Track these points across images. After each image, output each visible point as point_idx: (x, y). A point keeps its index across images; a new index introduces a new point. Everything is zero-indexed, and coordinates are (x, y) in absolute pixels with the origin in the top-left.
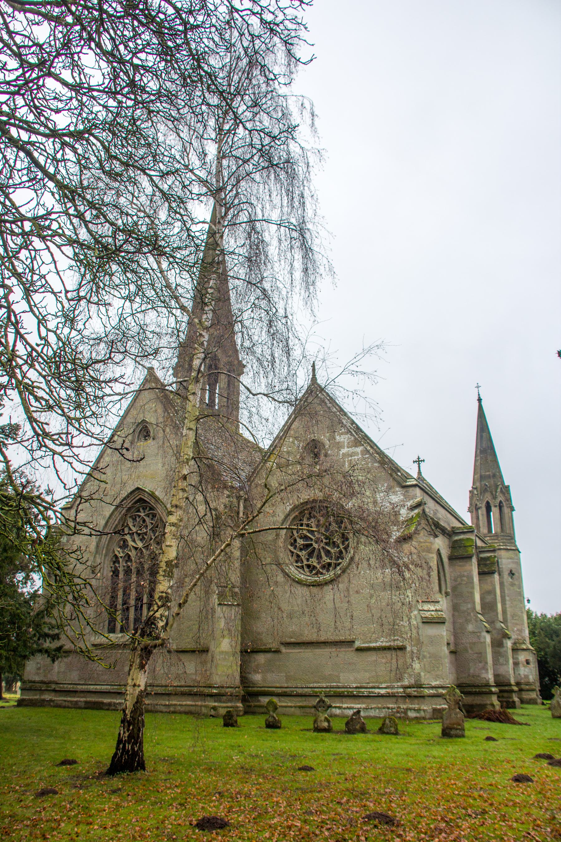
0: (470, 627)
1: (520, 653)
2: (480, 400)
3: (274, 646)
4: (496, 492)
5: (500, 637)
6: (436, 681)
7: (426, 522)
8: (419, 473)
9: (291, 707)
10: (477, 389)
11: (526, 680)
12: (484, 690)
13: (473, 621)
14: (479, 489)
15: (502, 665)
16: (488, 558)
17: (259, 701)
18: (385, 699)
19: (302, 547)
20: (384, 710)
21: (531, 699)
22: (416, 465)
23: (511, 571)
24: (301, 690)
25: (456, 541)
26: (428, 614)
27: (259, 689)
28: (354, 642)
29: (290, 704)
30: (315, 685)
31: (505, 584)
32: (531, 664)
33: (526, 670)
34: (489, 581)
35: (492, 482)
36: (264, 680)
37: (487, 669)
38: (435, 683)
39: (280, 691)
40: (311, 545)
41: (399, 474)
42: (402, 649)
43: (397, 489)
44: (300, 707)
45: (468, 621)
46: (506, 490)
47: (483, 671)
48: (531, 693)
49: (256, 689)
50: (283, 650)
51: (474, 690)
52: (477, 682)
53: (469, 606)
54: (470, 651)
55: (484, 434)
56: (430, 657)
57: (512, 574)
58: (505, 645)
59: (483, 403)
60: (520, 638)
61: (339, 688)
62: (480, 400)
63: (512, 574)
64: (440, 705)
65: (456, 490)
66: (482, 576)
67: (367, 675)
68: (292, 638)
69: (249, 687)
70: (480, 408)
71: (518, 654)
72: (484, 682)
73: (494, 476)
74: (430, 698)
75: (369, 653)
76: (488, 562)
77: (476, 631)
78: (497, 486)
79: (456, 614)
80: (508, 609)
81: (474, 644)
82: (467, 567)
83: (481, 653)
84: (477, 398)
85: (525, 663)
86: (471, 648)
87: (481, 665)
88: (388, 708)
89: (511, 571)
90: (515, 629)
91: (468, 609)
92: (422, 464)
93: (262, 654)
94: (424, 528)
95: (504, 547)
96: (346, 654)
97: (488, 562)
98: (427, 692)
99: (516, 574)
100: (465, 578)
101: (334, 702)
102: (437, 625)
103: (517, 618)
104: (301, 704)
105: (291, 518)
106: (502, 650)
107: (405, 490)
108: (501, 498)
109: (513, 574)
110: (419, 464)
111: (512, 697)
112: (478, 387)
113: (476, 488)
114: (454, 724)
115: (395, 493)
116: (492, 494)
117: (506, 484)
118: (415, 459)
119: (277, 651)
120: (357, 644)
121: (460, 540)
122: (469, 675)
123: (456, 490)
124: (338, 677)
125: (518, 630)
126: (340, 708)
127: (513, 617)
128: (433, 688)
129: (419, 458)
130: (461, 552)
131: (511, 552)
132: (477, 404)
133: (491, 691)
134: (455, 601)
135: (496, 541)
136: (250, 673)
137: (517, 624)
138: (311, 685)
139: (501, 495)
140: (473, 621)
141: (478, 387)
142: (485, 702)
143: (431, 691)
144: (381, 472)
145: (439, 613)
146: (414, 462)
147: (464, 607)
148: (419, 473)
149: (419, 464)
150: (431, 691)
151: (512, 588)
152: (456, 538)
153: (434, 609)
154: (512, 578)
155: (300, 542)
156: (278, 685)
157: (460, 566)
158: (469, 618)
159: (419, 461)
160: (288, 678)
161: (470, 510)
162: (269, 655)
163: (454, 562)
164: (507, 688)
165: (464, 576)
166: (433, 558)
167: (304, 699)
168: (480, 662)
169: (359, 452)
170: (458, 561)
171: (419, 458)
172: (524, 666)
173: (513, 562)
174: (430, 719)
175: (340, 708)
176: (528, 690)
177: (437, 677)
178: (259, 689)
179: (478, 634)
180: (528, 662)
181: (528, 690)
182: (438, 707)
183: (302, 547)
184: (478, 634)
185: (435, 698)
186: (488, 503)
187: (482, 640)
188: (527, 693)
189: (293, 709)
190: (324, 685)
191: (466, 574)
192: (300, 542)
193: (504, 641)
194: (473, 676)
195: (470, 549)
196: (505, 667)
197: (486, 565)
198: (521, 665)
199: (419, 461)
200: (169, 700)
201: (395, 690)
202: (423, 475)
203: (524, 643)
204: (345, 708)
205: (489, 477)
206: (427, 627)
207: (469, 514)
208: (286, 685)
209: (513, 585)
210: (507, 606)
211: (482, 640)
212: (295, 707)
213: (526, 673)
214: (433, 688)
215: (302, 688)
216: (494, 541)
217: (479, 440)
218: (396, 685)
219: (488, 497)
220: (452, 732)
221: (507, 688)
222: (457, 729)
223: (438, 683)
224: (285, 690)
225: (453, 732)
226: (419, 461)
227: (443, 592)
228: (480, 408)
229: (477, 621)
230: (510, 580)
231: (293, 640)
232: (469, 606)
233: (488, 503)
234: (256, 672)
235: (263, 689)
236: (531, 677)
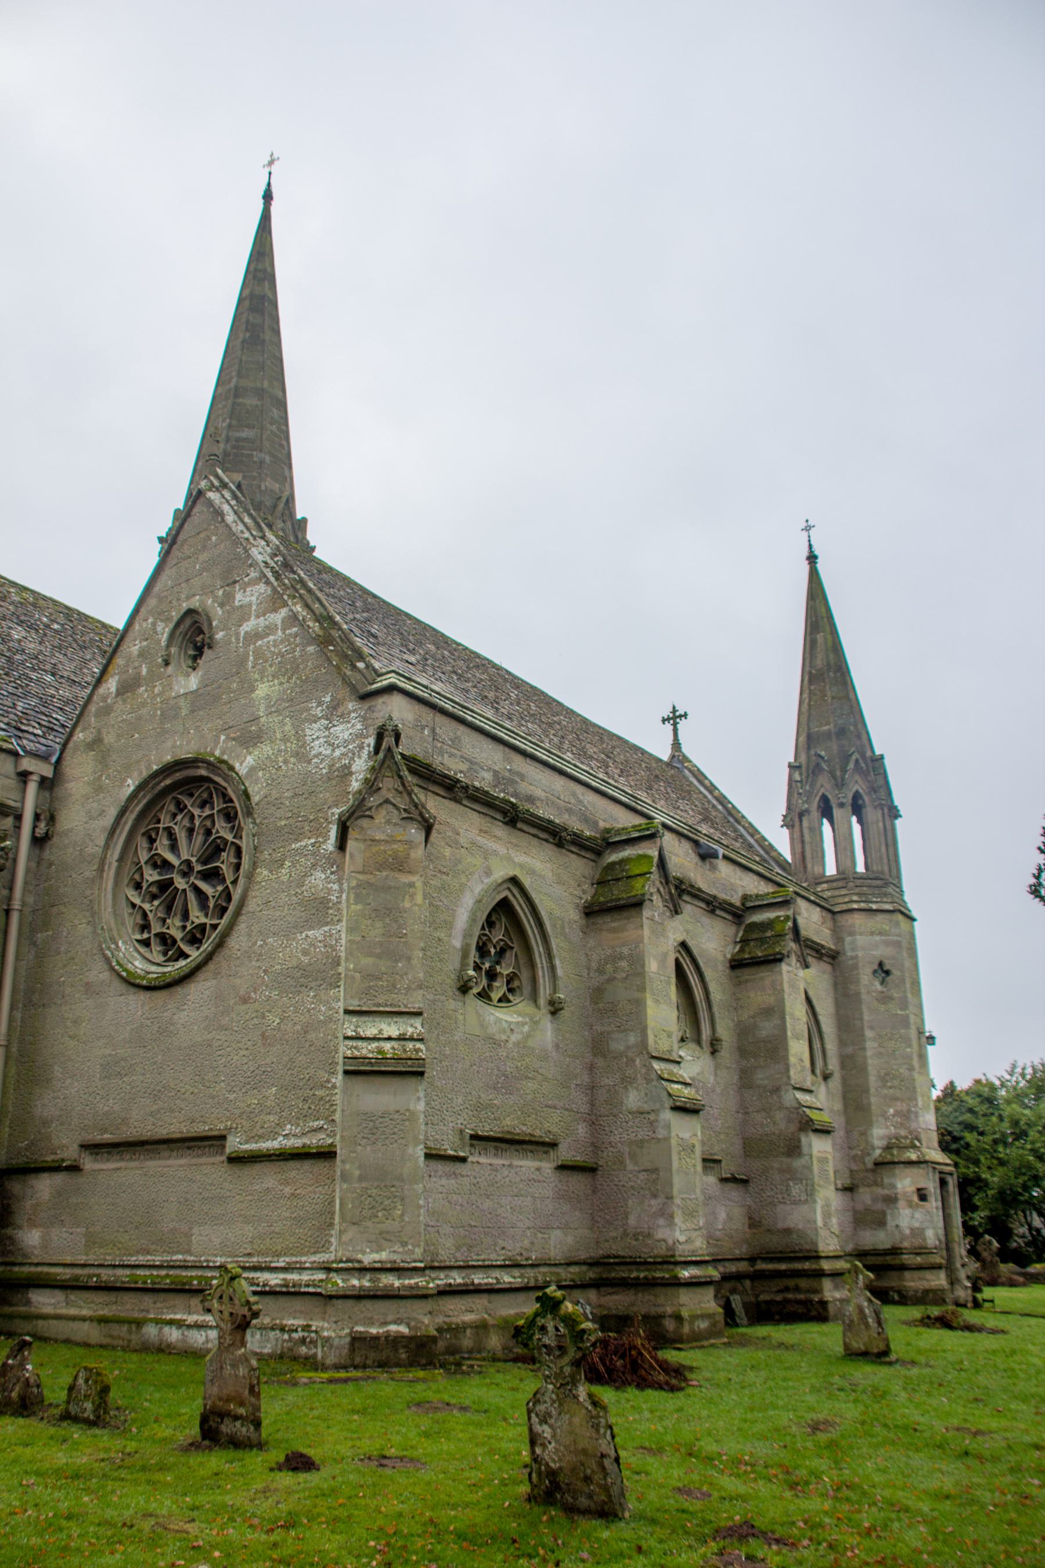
0: (633, 1099)
1: (899, 1170)
2: (812, 558)
3: (70, 1152)
4: (844, 770)
5: (793, 1127)
6: (380, 1249)
7: (398, 784)
8: (676, 745)
9: (83, 1319)
10: (805, 534)
11: (917, 1242)
12: (658, 1275)
13: (640, 1080)
14: (804, 769)
15: (796, 1203)
16: (769, 925)
17: (28, 1302)
18: (283, 1301)
19: (154, 889)
20: (272, 1334)
21: (927, 1292)
22: (669, 727)
23: (881, 964)
24: (110, 1271)
25: (614, 863)
26: (367, 1049)
27: (33, 1269)
28: (223, 1138)
29: (85, 1312)
30: (142, 1259)
31: (864, 996)
32: (932, 1199)
33: (917, 1215)
34: (767, 982)
35: (835, 747)
36: (45, 1244)
37: (672, 1216)
38: (376, 1256)
39: (65, 1273)
40: (171, 882)
41: (361, 665)
42: (327, 1155)
43: (350, 706)
44: (103, 1320)
45: (627, 1081)
46: (875, 766)
47: (661, 1221)
48: (928, 1275)
49: (26, 1269)
50: (88, 1163)
51: (634, 1275)
52: (646, 1252)
53: (632, 1039)
54: (630, 1166)
55: (820, 637)
56: (361, 1179)
57: (883, 971)
58: (805, 1150)
59: (820, 566)
60: (903, 1133)
61: (186, 1267)
62: (812, 558)
63: (883, 971)
64: (385, 1323)
65: (753, 774)
66: (738, 972)
67: (249, 1230)
68: (105, 1130)
69: (14, 1264)
70: (814, 577)
71: (894, 1176)
72: (661, 1251)
73: (841, 732)
74: (350, 1303)
75: (257, 1168)
76: (769, 934)
77: (646, 1107)
78: (847, 757)
79: (600, 1062)
80: (870, 1061)
81: (640, 1144)
82: (630, 933)
83: (656, 1170)
84: (805, 553)
85: (916, 1199)
86: (633, 1156)
87: (655, 1204)
88: (282, 1329)
89: (881, 964)
90: (891, 1111)
91: (628, 1048)
92: (682, 724)
93: (45, 1175)
94: (387, 801)
95: (863, 905)
96: (209, 1171)
97: (769, 934)
98: (685, 1274)
99: (896, 972)
100: (623, 964)
101: (173, 1309)
102: (396, 1083)
103: (896, 1083)
104: (104, 1312)
105: (133, 816)
106: (798, 1163)
107: (366, 705)
108: (857, 785)
109: (887, 973)
110: (675, 725)
111: (818, 1291)
112: (808, 528)
113: (799, 767)
114: (228, 1400)
115: (344, 717)
116: (834, 777)
117: (878, 752)
118: (667, 712)
119: (74, 1168)
120: (235, 1144)
121: (622, 862)
122: (625, 1234)
123: (753, 774)
124: (188, 1235)
125: (897, 1113)
126: (179, 1324)
127: (883, 1079)
128: (363, 1270)
129: (674, 711)
130: (618, 893)
131: (880, 917)
132: (805, 568)
133: (676, 1277)
134: (599, 1028)
135: (843, 892)
136: (20, 1228)
137: (896, 1099)
138: (133, 1260)
139: (857, 777)
140: (640, 1080)
141: (808, 528)
142: (660, 1310)
143: (355, 1282)
144: (318, 667)
145: (410, 1045)
146: (664, 721)
147: (617, 1045)
148: (676, 745)
149: (675, 725)
150: (355, 1282)
151: (882, 1008)
152: (614, 857)
153: (395, 1034)
154: (882, 983)
155: (151, 876)
156: (68, 1259)
157: (614, 930)
158: (629, 1072)
159: (674, 718)
160: (91, 1241)
161: (788, 822)
162: (59, 1178)
163: (600, 920)
164: (807, 1265)
165: (621, 957)
166: (412, 885)
167: (112, 1297)
168: (655, 1196)
169: (279, 623)
170: (607, 918)
171: (674, 711)
172: (910, 1204)
173: (887, 944)
174: (337, 1367)
175: (179, 1324)
176: (920, 1268)
177: (382, 1239)
178: (33, 1269)
179: (652, 1117)
180: (922, 1196)
181: (920, 1268)
182: (374, 1331)
183: (154, 889)
184: (652, 1117)
185: (368, 1304)
186: (825, 799)
187: (661, 1133)
188: (917, 1274)
189: (86, 1326)
190: (157, 1259)
191: (626, 951)
192: (151, 876)
193: (804, 1139)
194: (636, 1237)
195: (638, 883)
196: (806, 1207)
197: (762, 941)
198: (901, 1203)
199: (674, 718)
200: (438, 1285)
201: (305, 1277)
202: (685, 749)
203: (914, 1147)
204: (189, 1327)
205: (828, 735)
206: (359, 1085)
207: (785, 831)
208: (82, 1259)
209: (885, 999)
210: (869, 1053)
211: (661, 1133)
212: (91, 1319)
213: (916, 1225)
214: (363, 1270)
215: (114, 1266)
216: (837, 893)
217: (807, 655)
218: (308, 1260)
219: (824, 785)
220: (223, 1428)
221: (807, 1265)
222: (236, 1418)
223: (384, 1256)
224: (79, 1271)
225: (227, 1427)
226: (675, 718)
227: (542, 1001)
228: (814, 577)
229: (649, 1081)
230: (879, 987)
231: (107, 1137)
232: (632, 1039)
233: (825, 799)
234: (33, 1224)
235: (40, 1269)
236: (59, 1236)
